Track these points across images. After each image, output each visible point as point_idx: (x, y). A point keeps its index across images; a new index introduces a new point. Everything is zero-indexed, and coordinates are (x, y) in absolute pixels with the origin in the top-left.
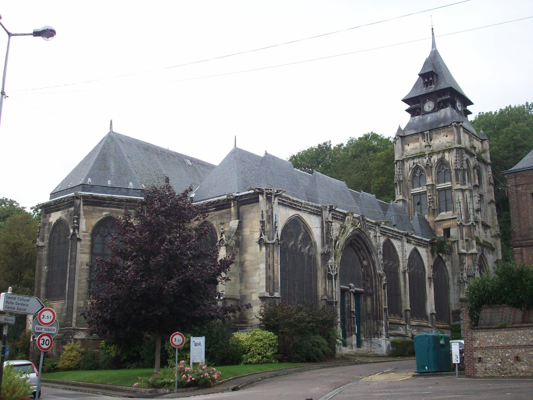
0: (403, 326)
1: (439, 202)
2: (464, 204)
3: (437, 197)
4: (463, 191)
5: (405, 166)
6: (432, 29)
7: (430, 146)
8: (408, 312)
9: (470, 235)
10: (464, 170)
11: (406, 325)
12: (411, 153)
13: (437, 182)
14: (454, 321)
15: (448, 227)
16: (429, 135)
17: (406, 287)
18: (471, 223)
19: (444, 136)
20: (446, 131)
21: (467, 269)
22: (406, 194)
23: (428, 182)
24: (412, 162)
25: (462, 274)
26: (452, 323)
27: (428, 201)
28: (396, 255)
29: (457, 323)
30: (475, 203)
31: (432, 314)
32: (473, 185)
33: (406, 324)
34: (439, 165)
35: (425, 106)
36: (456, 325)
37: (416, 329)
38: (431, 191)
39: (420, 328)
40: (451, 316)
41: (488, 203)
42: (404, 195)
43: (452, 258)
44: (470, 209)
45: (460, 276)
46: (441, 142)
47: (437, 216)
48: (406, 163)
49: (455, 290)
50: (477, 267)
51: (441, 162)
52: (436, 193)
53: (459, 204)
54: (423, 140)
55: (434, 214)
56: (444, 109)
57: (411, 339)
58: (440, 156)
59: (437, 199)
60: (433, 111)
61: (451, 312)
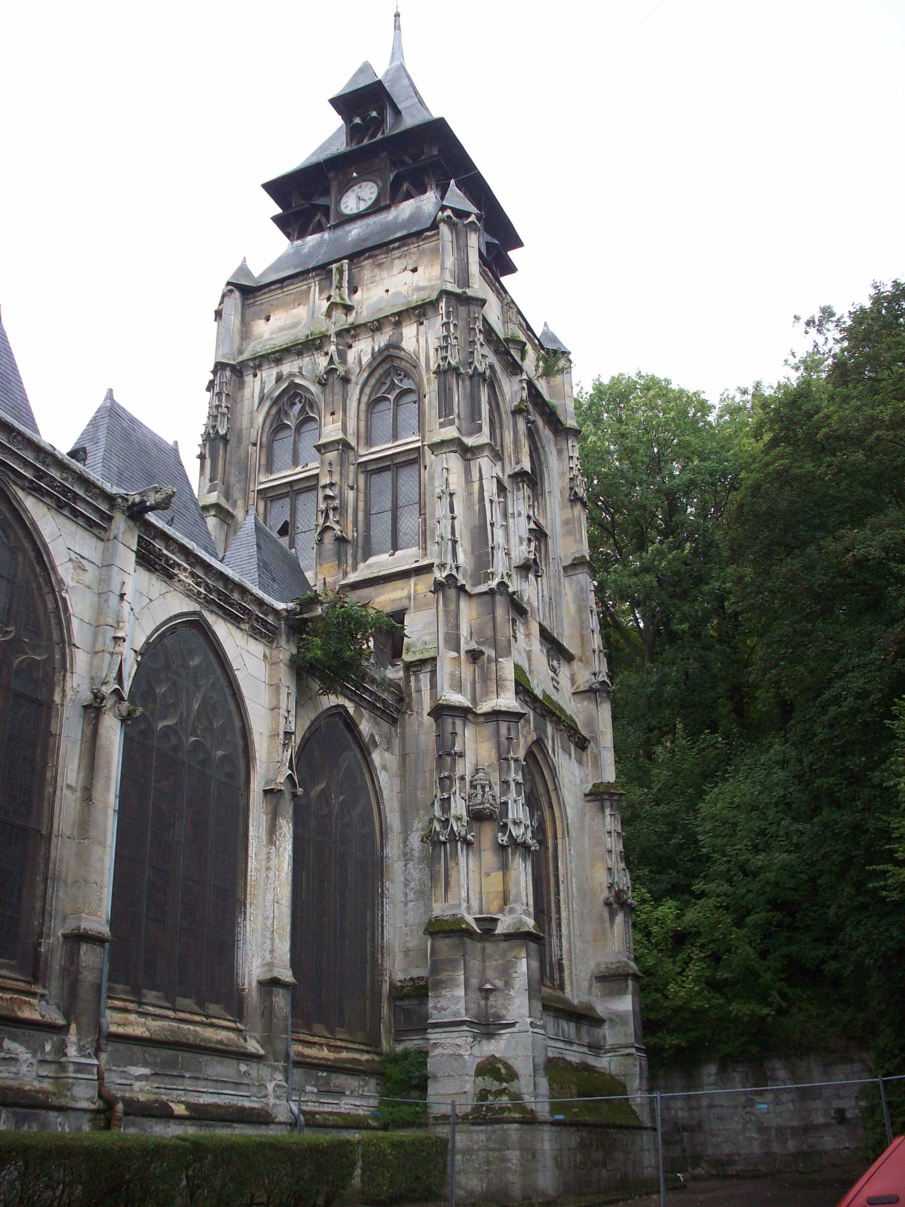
0: (39, 1035)
1: (368, 514)
2: (469, 507)
3: (361, 496)
4: (467, 453)
5: (247, 392)
6: (397, 15)
7: (348, 309)
8: (84, 947)
9: (490, 633)
10: (477, 377)
11: (63, 1030)
12: (274, 342)
13: (362, 441)
14: (399, 1036)
15: (397, 607)
16: (346, 274)
17: (97, 795)
18: (497, 580)
19: (405, 269)
20: (415, 254)
21: (471, 782)
22: (237, 494)
23: (327, 437)
24: (274, 372)
25: (446, 804)
26: (385, 1046)
27: (322, 506)
28: (50, 605)
29: (412, 1043)
30: (514, 541)
31: (271, 984)
32: (509, 471)
33: (61, 1021)
34: (377, 375)
35: (344, 200)
36: (406, 1054)
37: (145, 1064)
38: (336, 469)
39: (182, 1056)
40: (385, 1011)
41: (565, 568)
42: (227, 496)
43: (403, 739)
44: (492, 525)
45: (437, 812)
46: (390, 293)
47: (355, 568)
48: (249, 379)
49: (412, 885)
50: (515, 776)
51: (386, 366)
52: (356, 480)
53: (446, 500)
54: (325, 295)
55: (340, 558)
56: (412, 201)
57: (86, 1128)
58: (382, 339)
59: (361, 505)
60: (376, 209)
61: (386, 987)
